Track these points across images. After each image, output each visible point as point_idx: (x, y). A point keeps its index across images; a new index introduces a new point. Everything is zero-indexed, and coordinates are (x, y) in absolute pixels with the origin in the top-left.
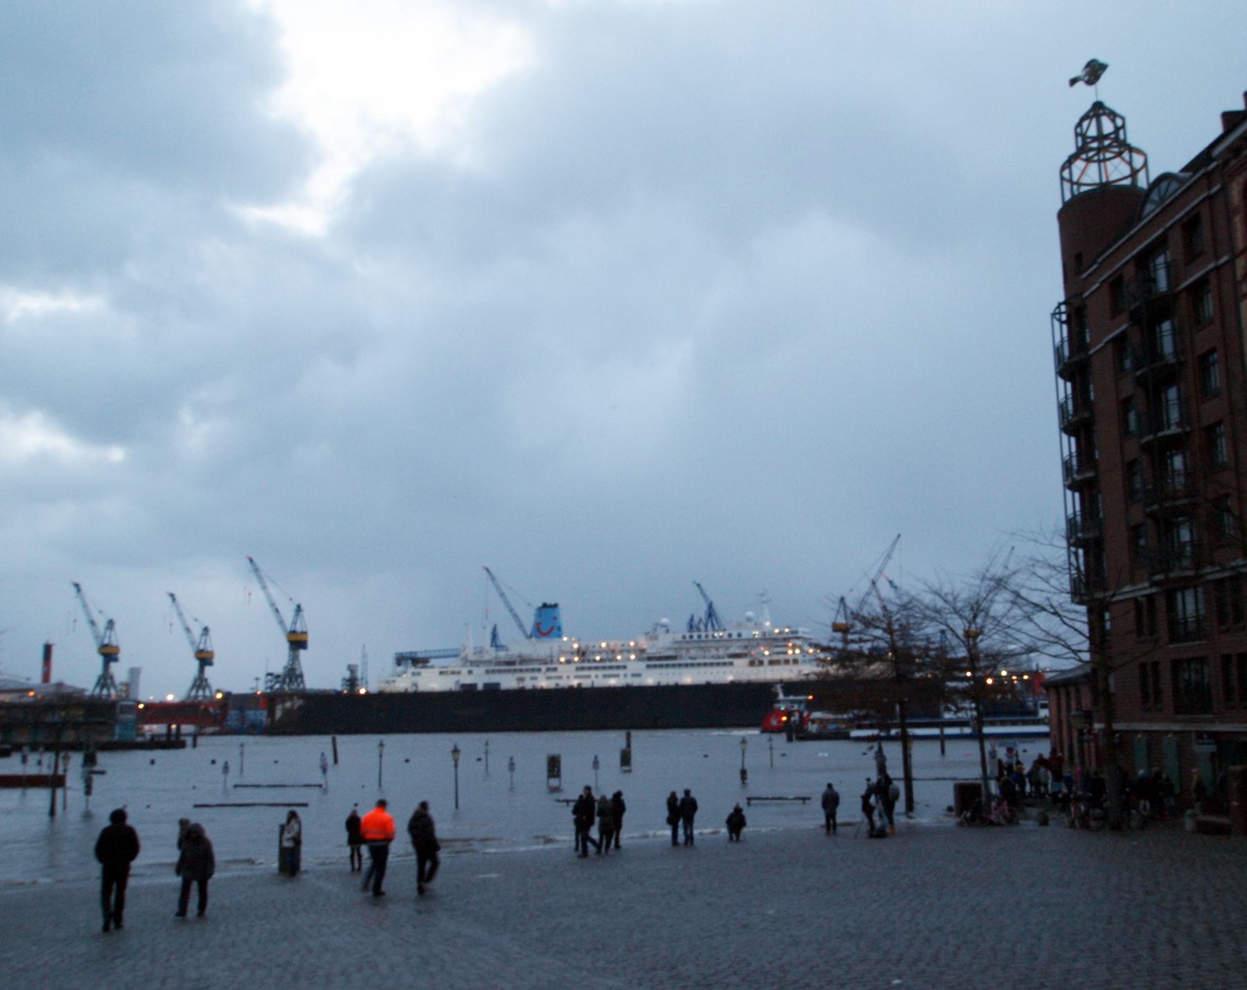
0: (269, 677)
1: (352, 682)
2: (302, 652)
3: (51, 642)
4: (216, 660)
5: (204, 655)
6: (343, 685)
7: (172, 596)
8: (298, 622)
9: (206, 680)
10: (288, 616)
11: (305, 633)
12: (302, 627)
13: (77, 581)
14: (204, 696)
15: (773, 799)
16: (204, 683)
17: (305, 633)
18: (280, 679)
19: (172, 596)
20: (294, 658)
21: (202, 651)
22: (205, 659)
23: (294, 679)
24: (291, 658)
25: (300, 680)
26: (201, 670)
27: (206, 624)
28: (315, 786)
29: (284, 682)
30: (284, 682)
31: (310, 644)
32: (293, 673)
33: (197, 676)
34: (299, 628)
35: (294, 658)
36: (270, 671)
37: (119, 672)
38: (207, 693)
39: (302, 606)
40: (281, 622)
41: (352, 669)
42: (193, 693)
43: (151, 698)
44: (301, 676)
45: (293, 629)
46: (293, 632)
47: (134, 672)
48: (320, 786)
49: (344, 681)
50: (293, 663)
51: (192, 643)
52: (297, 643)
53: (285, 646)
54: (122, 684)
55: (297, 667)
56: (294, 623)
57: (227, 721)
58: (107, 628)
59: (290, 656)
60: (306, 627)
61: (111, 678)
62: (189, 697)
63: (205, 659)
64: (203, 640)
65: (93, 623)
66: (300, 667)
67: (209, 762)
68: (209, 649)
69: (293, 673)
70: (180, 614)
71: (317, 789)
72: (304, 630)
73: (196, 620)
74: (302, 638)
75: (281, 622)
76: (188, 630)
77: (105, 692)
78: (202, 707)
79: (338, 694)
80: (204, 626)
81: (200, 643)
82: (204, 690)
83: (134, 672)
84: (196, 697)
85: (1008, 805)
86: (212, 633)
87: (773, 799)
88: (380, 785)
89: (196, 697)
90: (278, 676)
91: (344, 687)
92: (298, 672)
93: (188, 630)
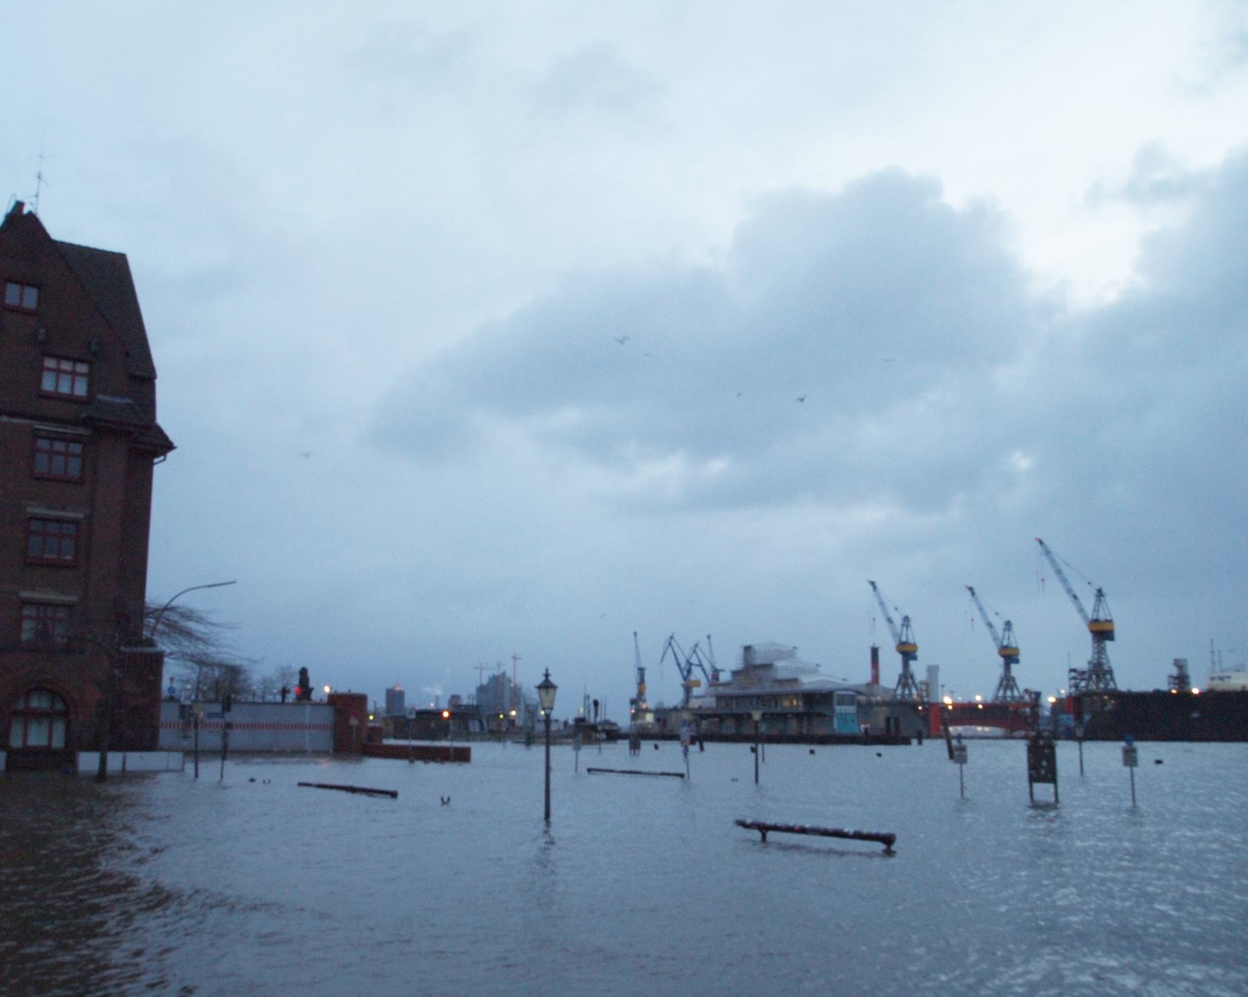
0: (1073, 674)
1: (1181, 679)
2: (1108, 644)
3: (876, 646)
4: (1021, 657)
5: (1008, 652)
6: (1169, 683)
7: (873, 583)
8: (1101, 610)
9: (1013, 679)
10: (1089, 603)
11: (1110, 621)
12: (1106, 615)
13: (970, 585)
14: (1013, 697)
15: (859, 836)
16: (1012, 683)
17: (1110, 621)
18: (1086, 676)
19: (873, 583)
20: (1100, 651)
21: (904, 644)
22: (1009, 656)
23: (1101, 676)
24: (1096, 651)
25: (1108, 677)
26: (906, 665)
27: (1007, 618)
28: (675, 775)
29: (1090, 678)
30: (1090, 678)
31: (1118, 633)
32: (1099, 670)
33: (1003, 676)
34: (1102, 616)
35: (1100, 651)
36: (1073, 666)
37: (919, 669)
38: (1016, 693)
39: (1105, 591)
40: (1081, 610)
41: (1180, 664)
42: (1001, 693)
43: (960, 698)
44: (1110, 672)
45: (1095, 617)
46: (1096, 621)
47: (933, 670)
48: (682, 776)
49: (1172, 680)
50: (1099, 657)
51: (995, 639)
52: (1102, 633)
53: (1089, 637)
54: (921, 683)
55: (1104, 661)
56: (1096, 610)
57: (1039, 725)
58: (1005, 630)
59: (1094, 648)
60: (1110, 615)
61: (912, 677)
62: (997, 697)
63: (1009, 656)
64: (1006, 637)
65: (890, 620)
66: (1108, 661)
67: (812, 756)
68: (1014, 645)
69: (1099, 670)
70: (981, 609)
71: (679, 779)
72: (1109, 618)
73: (896, 609)
74: (1106, 627)
75: (1081, 610)
76: (990, 625)
77: (1009, 693)
78: (1011, 709)
79: (1158, 695)
80: (1007, 620)
81: (1003, 638)
82: (1012, 691)
83: (933, 670)
84: (1005, 697)
85: (1078, 929)
86: (1014, 628)
87: (859, 836)
88: (757, 780)
89: (1005, 697)
90: (1083, 673)
91: (1172, 686)
92: (1106, 667)
93: (990, 625)
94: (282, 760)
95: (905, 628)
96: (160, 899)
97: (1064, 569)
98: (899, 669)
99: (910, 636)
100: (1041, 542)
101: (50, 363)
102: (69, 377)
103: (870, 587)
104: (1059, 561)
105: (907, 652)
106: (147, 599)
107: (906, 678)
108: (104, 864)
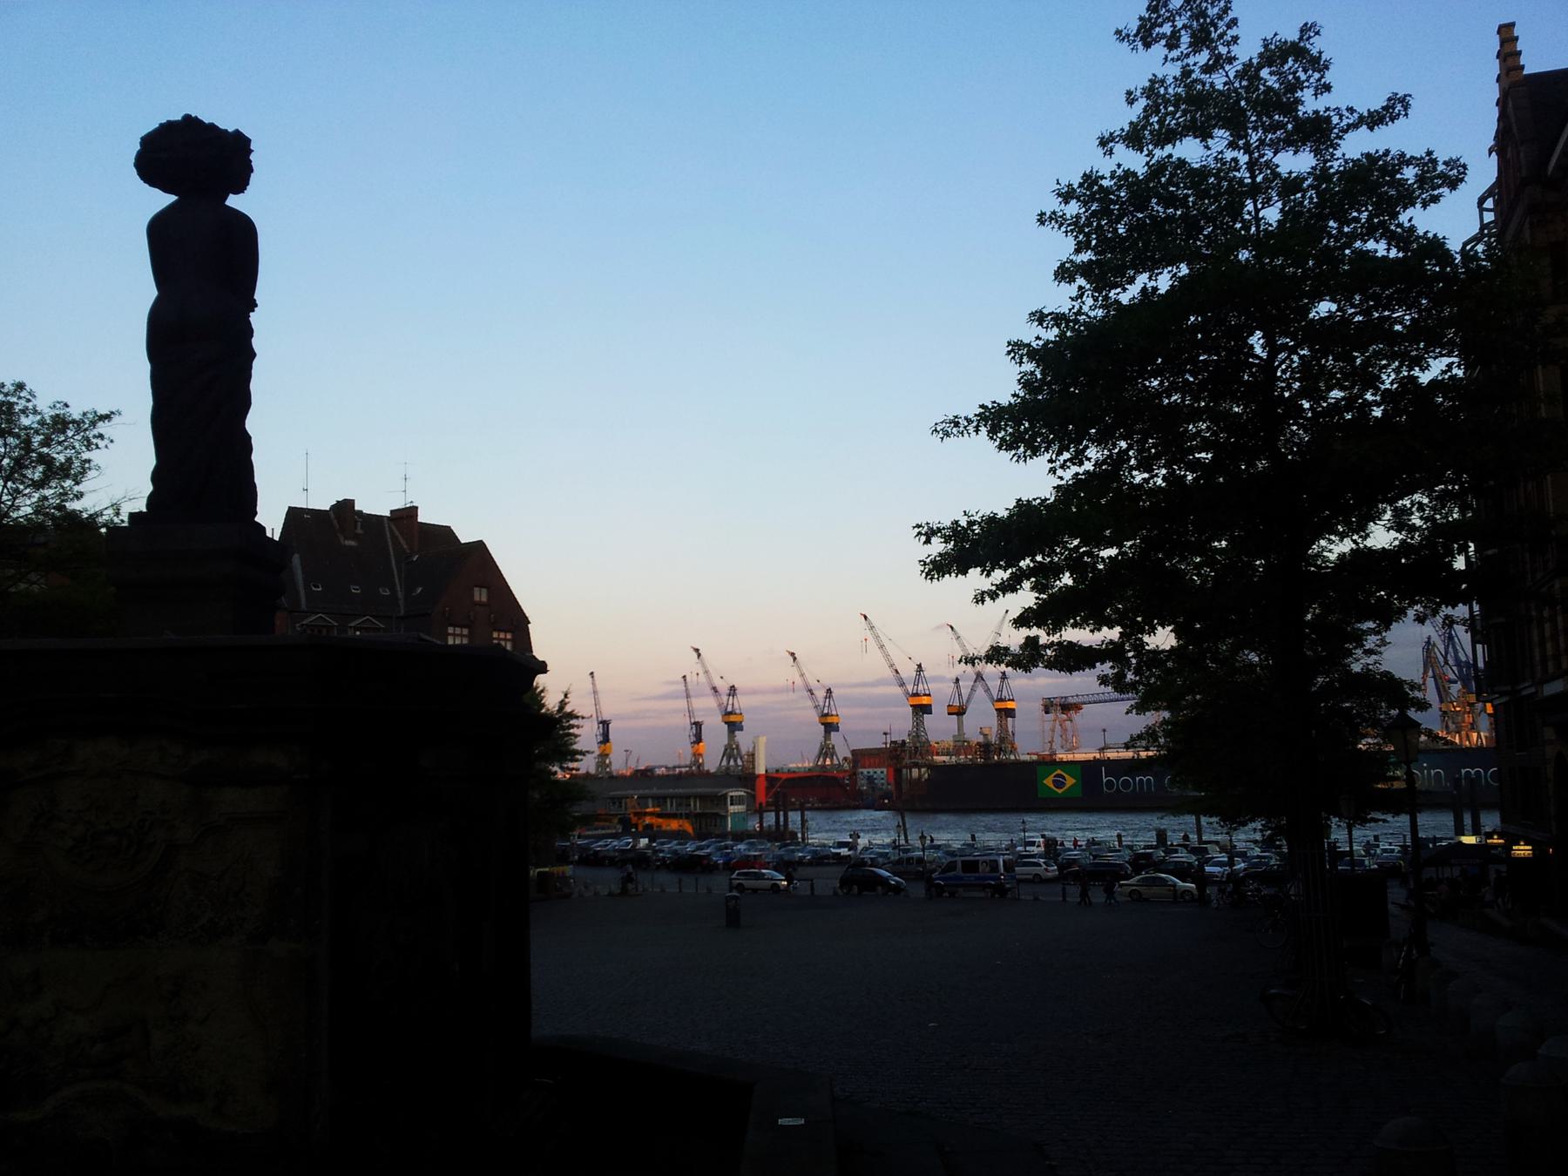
8: (920, 685)
9: (1055, 274)
21: (728, 714)
38: (836, 762)
83: (569, 702)
94: (756, 764)
95: (731, 697)
96: (766, 771)
97: (888, 645)
98: (724, 740)
99: (736, 706)
100: (866, 617)
101: (450, 630)
102: (460, 638)
103: (695, 655)
104: (882, 637)
105: (734, 727)
106: (1452, 815)
107: (731, 751)
108: (1463, 635)
